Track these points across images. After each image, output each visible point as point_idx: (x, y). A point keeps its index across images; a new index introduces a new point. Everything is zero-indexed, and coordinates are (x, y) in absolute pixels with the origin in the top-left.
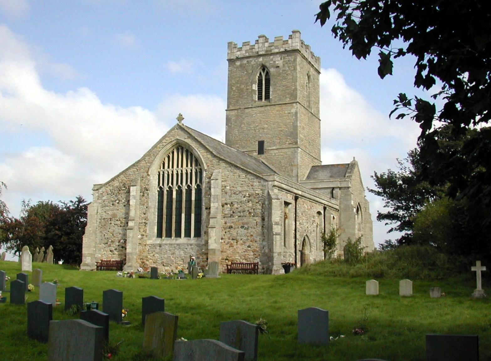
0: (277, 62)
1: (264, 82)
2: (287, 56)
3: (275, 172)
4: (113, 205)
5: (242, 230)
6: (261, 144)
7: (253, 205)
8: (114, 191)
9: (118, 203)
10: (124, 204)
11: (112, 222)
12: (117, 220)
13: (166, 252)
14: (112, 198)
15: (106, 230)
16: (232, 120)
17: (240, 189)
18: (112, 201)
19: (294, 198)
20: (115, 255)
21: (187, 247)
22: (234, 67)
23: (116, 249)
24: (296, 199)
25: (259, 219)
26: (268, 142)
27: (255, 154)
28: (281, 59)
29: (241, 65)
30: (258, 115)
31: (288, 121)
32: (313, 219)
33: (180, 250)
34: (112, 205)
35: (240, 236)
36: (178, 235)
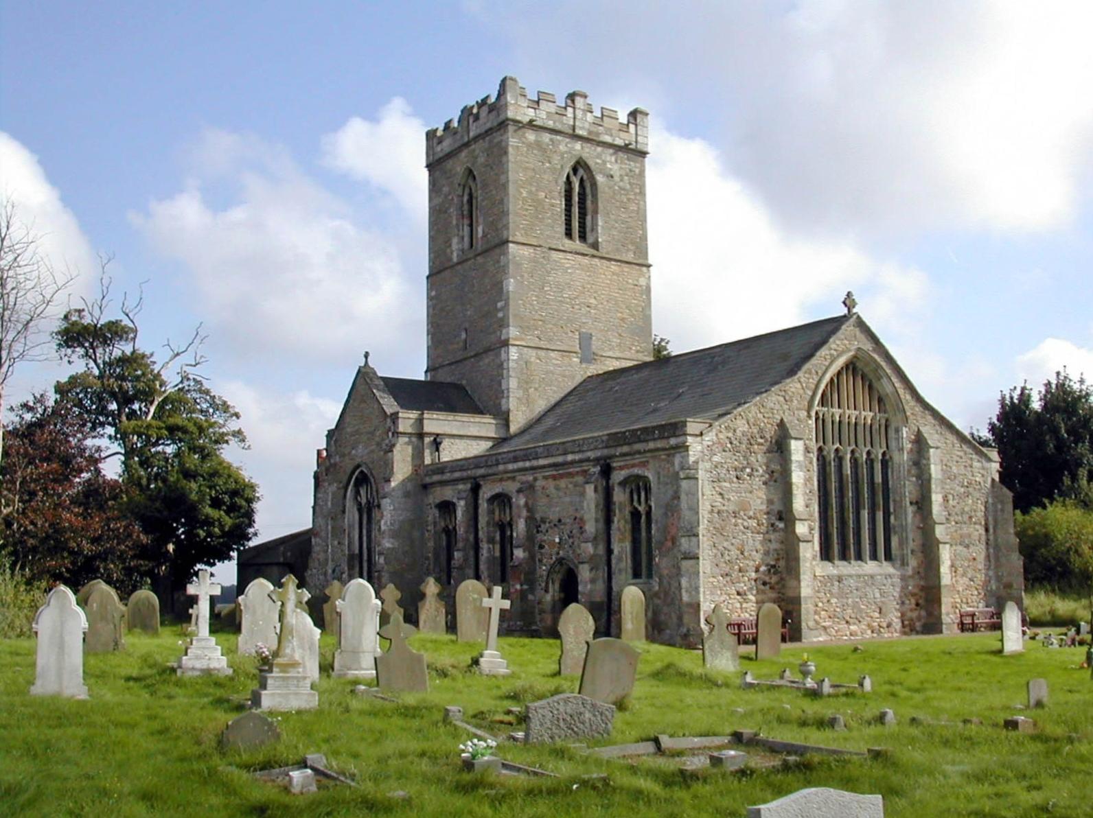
6: (585, 340)
9: (750, 475)
10: (764, 479)
12: (750, 518)
13: (851, 592)
20: (750, 604)
21: (885, 582)
22: (523, 143)
23: (751, 589)
26: (598, 339)
27: (575, 359)
28: (616, 161)
29: (538, 144)
34: (735, 480)
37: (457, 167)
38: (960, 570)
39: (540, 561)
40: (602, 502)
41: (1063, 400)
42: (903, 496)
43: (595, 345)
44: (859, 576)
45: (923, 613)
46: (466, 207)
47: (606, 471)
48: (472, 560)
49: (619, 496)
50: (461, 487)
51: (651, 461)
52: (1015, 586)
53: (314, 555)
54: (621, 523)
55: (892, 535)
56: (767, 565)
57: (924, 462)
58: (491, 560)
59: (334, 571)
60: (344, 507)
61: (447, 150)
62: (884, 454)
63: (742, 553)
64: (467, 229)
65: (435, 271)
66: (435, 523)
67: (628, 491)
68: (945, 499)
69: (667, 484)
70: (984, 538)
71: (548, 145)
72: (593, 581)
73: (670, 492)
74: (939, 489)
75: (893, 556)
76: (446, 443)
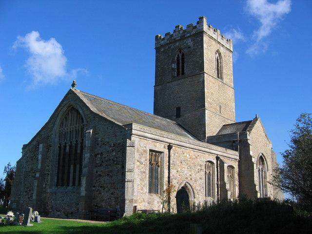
0: (189, 44)
1: (180, 61)
5: (108, 178)
6: (178, 109)
17: (107, 140)
19: (167, 148)
24: (170, 147)
28: (192, 41)
32: (200, 168)
36: (68, 185)
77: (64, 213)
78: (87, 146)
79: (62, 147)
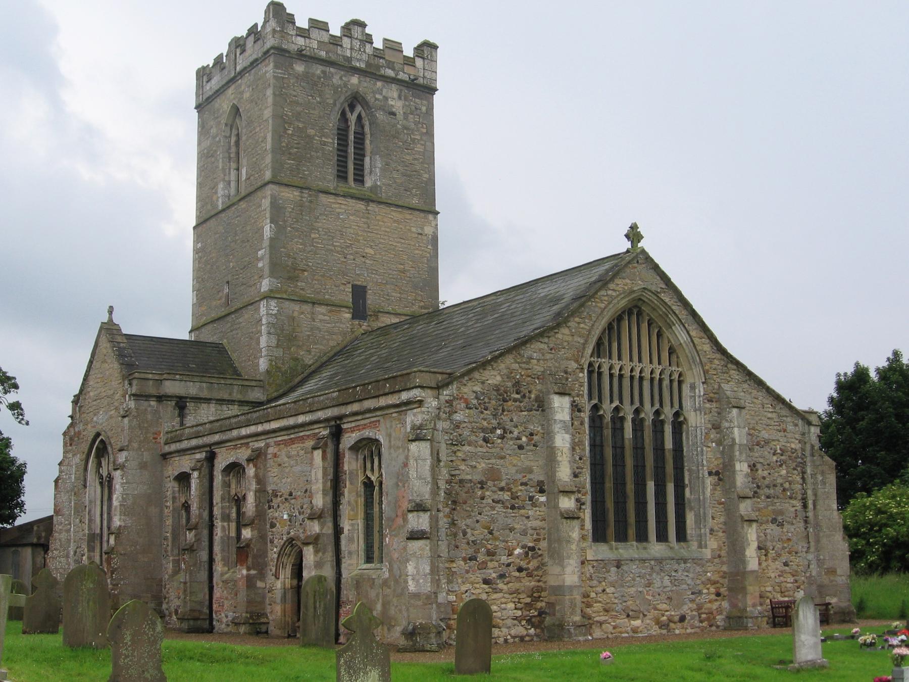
2: (413, 96)
3: (408, 374)
4: (486, 440)
5: (774, 527)
6: (359, 292)
7: (788, 473)
8: (486, 400)
9: (502, 437)
11: (487, 493)
12: (502, 489)
14: (485, 419)
15: (469, 516)
16: (287, 214)
18: (484, 430)
25: (798, 505)
28: (400, 98)
30: (351, 217)
31: (417, 252)
33: (662, 574)
34: (481, 442)
35: (772, 541)
36: (642, 537)
37: (224, 105)
38: (772, 553)
39: (272, 542)
40: (331, 471)
41: (896, 372)
42: (700, 464)
43: (372, 299)
44: (643, 561)
45: (725, 604)
46: (233, 149)
47: (337, 434)
48: (205, 544)
49: (350, 463)
50: (198, 456)
51: (382, 420)
52: (839, 572)
53: (56, 535)
54: (352, 495)
55: (687, 511)
56: (523, 547)
57: (726, 425)
58: (226, 540)
59: (75, 552)
60: (85, 480)
61: (216, 88)
62: (677, 415)
63: (491, 533)
64: (233, 173)
65: (202, 220)
66: (174, 498)
67: (361, 457)
68: (753, 467)
69: (398, 448)
70: (801, 514)
71: (319, 78)
72: (319, 565)
73: (402, 458)
74: (744, 457)
75: (689, 537)
76: (190, 405)
77: (658, 622)
78: (737, 441)
79: (648, 423)
